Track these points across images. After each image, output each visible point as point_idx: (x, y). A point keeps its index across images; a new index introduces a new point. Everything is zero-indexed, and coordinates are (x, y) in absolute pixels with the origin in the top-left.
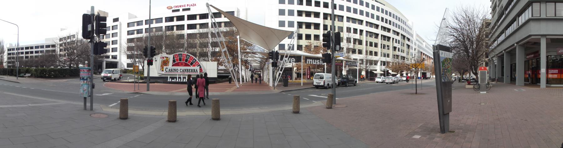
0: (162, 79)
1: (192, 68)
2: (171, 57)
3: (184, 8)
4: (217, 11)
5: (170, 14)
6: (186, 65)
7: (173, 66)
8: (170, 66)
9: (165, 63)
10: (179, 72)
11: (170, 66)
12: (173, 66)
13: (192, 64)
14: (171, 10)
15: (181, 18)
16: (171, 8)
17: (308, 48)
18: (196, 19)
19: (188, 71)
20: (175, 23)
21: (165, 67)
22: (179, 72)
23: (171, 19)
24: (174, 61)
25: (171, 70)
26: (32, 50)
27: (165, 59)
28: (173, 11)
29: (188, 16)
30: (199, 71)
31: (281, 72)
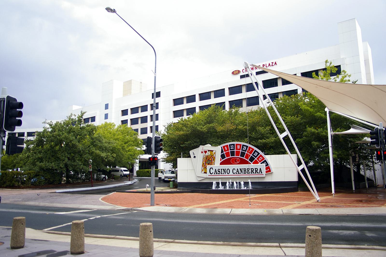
0: (202, 187)
1: (252, 166)
2: (218, 150)
3: (258, 70)
4: (279, 77)
5: (237, 81)
6: (243, 162)
7: (221, 164)
8: (217, 164)
9: (209, 160)
10: (231, 173)
11: (217, 164)
12: (221, 164)
13: (252, 159)
14: (238, 76)
15: (250, 87)
16: (239, 72)
17: (144, 120)
18: (276, 85)
19: (245, 171)
20: (245, 95)
21: (208, 167)
22: (231, 173)
23: (234, 90)
24: (223, 156)
25: (218, 172)
26: (144, 125)
27: (208, 153)
28: (242, 77)
29: (264, 82)
30: (264, 170)
31: (281, 136)
